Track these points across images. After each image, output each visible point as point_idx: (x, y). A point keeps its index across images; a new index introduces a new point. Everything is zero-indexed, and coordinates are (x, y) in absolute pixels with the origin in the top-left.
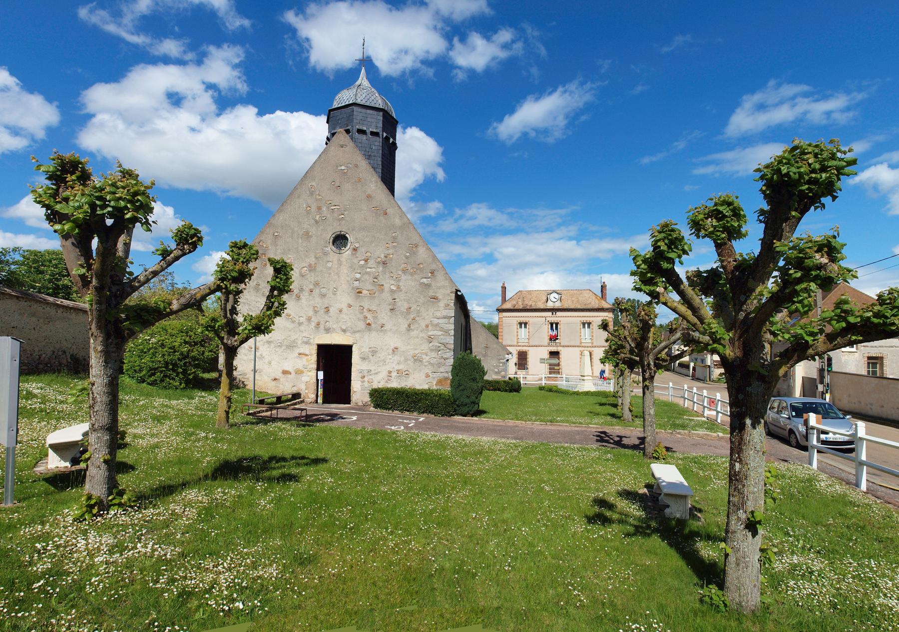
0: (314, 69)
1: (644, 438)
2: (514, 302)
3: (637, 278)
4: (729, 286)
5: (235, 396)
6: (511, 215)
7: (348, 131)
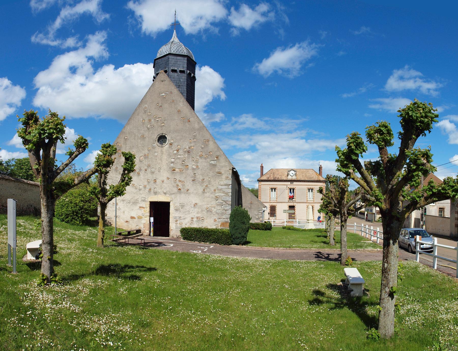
0: (145, 33)
1: (341, 254)
2: (268, 176)
3: (339, 164)
4: (384, 170)
5: (106, 230)
6: (266, 122)
7: (166, 72)
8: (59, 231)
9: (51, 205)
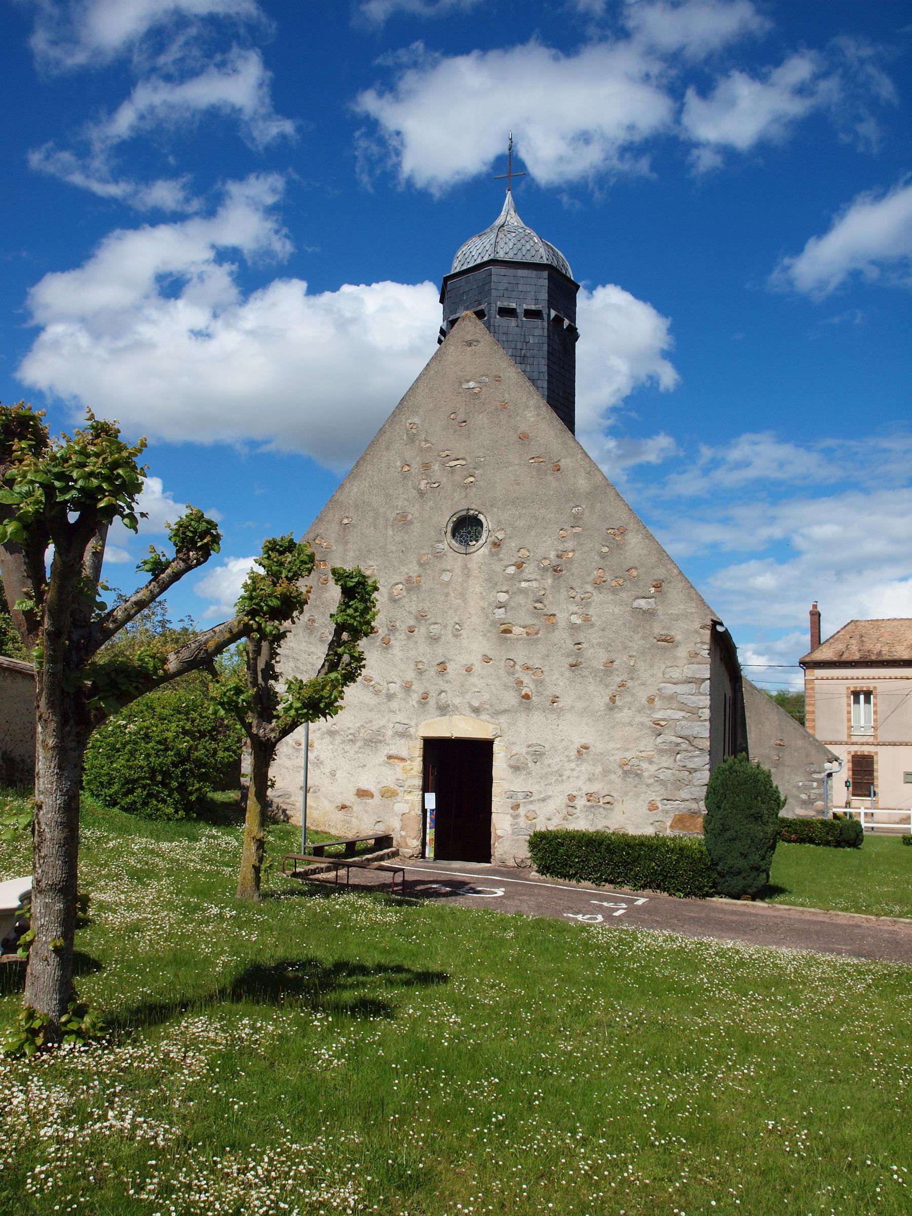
0: (409, 182)
2: (841, 647)
6: (828, 453)
7: (480, 314)
8: (98, 840)
9: (74, 744)
